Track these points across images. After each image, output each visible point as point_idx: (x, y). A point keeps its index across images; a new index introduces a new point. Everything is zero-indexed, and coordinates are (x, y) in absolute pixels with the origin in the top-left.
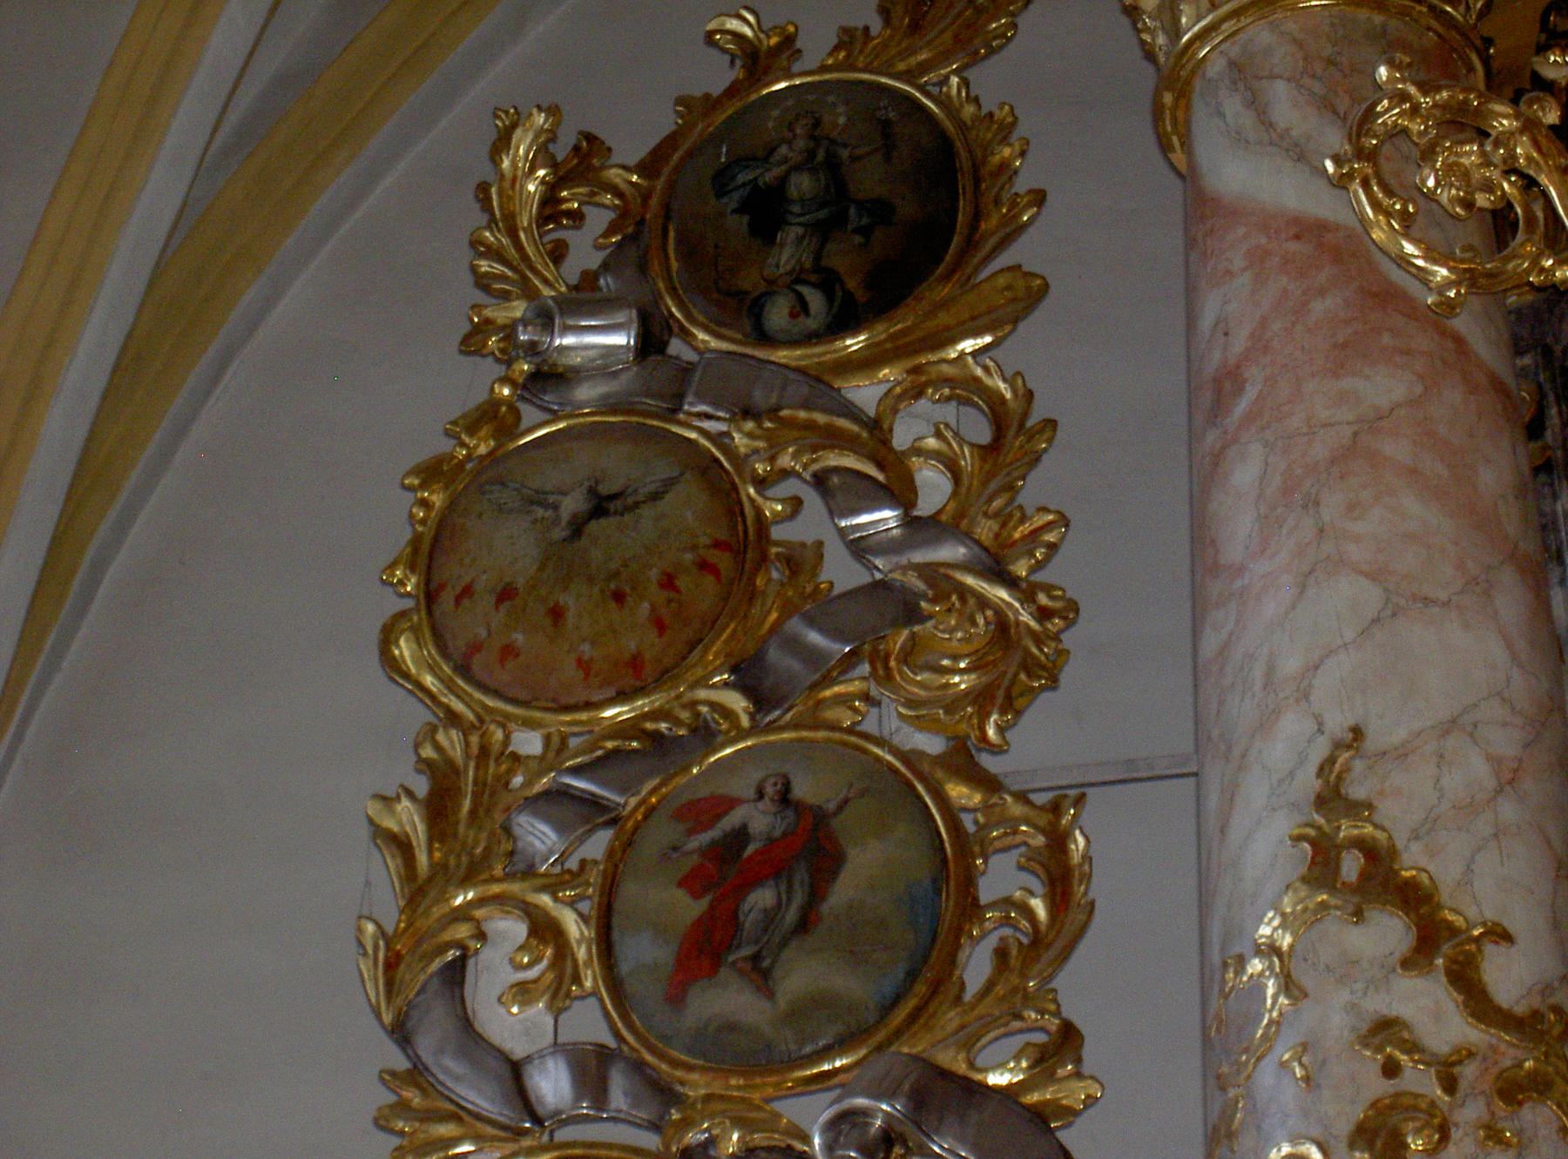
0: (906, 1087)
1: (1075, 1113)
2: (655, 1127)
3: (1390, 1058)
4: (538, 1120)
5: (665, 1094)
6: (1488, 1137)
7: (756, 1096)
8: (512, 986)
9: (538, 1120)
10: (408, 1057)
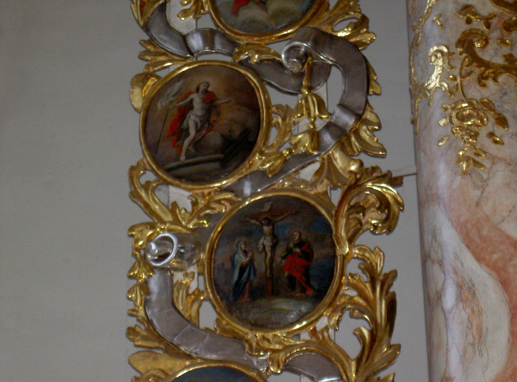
0: (312, 37)
1: (368, 45)
2: (230, 54)
3: (468, 18)
4: (192, 54)
5: (233, 44)
6: (501, 42)
7: (262, 43)
8: (182, 11)
9: (192, 54)
10: (149, 35)
